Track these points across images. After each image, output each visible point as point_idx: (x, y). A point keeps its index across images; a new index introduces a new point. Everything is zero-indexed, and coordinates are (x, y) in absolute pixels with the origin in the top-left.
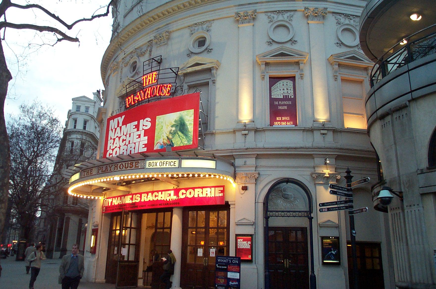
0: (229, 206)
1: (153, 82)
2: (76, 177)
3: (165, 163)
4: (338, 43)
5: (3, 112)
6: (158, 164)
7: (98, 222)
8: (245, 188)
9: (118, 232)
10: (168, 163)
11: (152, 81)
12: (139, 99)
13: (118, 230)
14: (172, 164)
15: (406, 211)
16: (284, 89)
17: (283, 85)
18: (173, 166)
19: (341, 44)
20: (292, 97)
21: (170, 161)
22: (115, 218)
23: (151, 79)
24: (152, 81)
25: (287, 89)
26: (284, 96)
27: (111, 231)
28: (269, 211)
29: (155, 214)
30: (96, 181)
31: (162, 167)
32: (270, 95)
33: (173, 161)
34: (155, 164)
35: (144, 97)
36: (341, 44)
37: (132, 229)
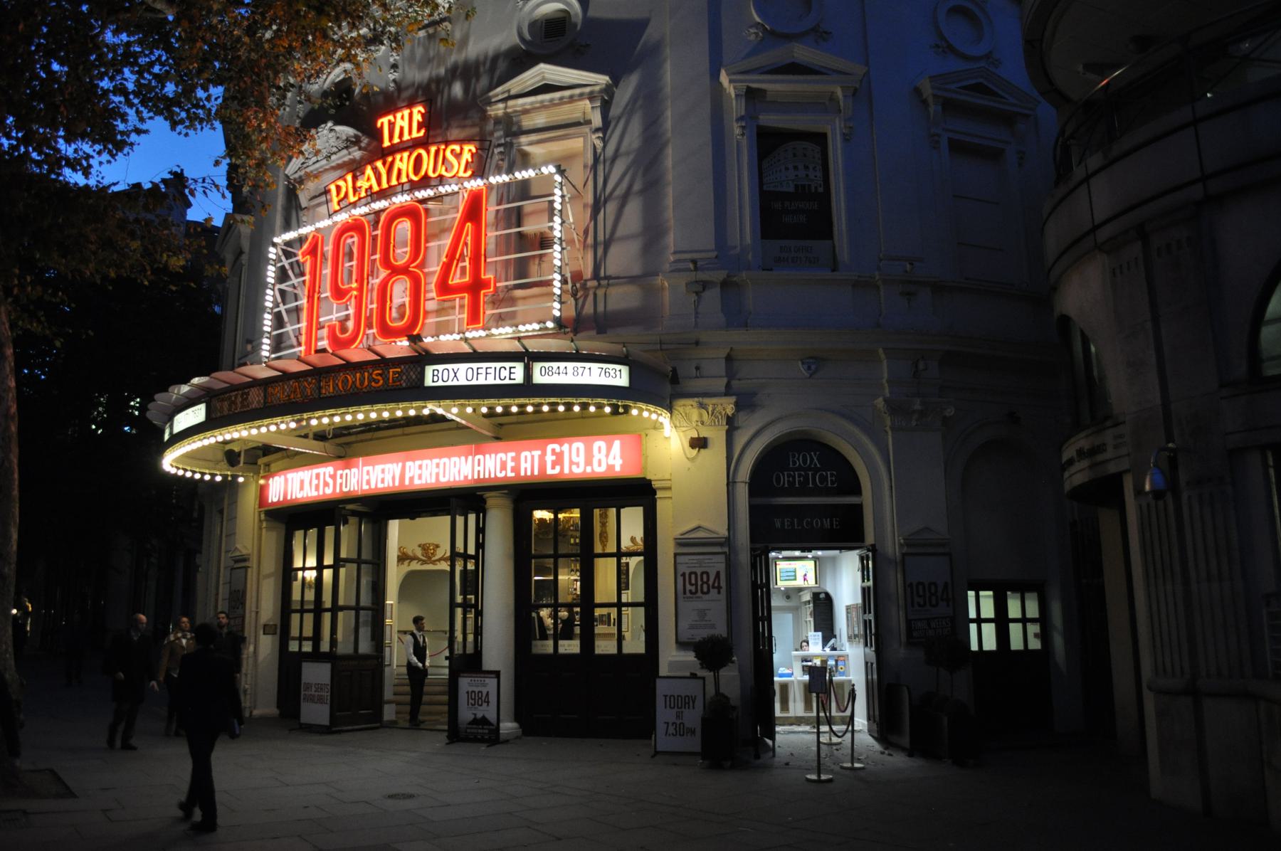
0: (654, 492)
1: (415, 135)
2: (194, 415)
3: (483, 371)
4: (937, 46)
5: (710, 62)
6: (461, 375)
7: (249, 547)
8: (699, 443)
9: (311, 575)
10: (492, 371)
11: (410, 133)
12: (371, 187)
13: (328, 567)
14: (505, 373)
15: (1185, 496)
16: (796, 168)
17: (795, 155)
18: (507, 381)
19: (948, 49)
20: (821, 190)
21: (498, 365)
22: (299, 535)
23: (406, 124)
24: (410, 133)
25: (806, 167)
26: (796, 186)
27: (288, 572)
28: (587, 519)
29: (448, 518)
30: (264, 430)
31: (474, 382)
32: (761, 184)
33: (507, 365)
34: (452, 375)
35: (389, 180)
36: (948, 49)
37: (363, 566)
